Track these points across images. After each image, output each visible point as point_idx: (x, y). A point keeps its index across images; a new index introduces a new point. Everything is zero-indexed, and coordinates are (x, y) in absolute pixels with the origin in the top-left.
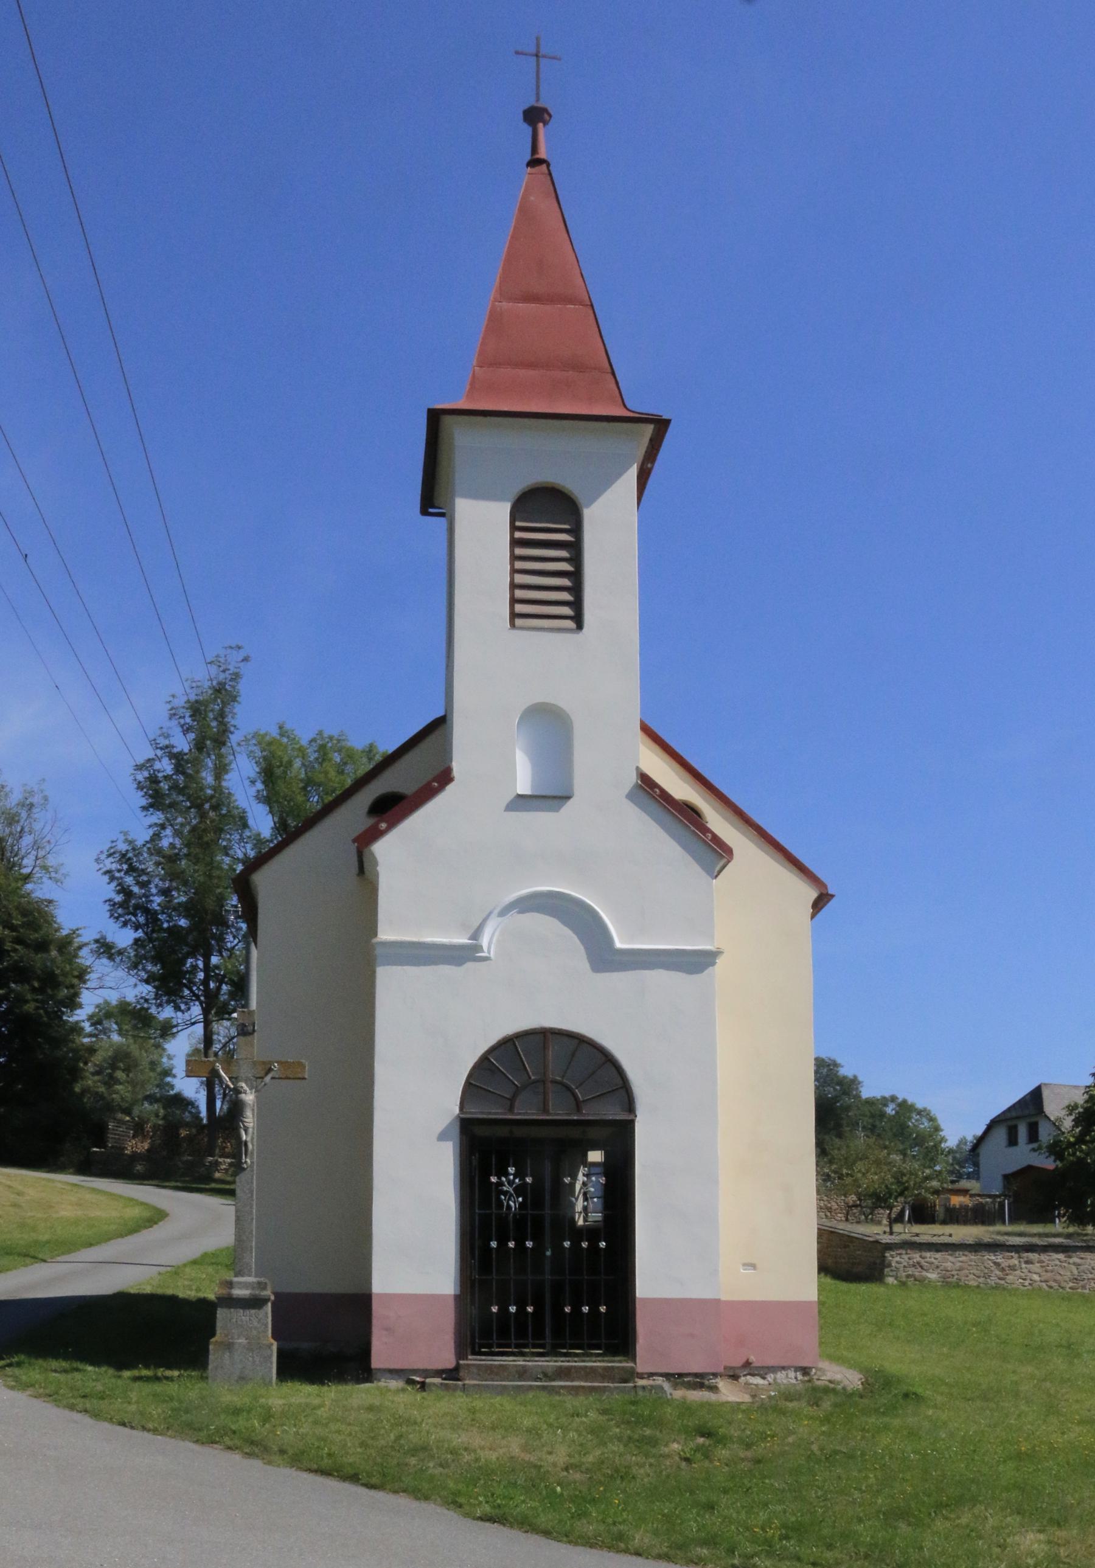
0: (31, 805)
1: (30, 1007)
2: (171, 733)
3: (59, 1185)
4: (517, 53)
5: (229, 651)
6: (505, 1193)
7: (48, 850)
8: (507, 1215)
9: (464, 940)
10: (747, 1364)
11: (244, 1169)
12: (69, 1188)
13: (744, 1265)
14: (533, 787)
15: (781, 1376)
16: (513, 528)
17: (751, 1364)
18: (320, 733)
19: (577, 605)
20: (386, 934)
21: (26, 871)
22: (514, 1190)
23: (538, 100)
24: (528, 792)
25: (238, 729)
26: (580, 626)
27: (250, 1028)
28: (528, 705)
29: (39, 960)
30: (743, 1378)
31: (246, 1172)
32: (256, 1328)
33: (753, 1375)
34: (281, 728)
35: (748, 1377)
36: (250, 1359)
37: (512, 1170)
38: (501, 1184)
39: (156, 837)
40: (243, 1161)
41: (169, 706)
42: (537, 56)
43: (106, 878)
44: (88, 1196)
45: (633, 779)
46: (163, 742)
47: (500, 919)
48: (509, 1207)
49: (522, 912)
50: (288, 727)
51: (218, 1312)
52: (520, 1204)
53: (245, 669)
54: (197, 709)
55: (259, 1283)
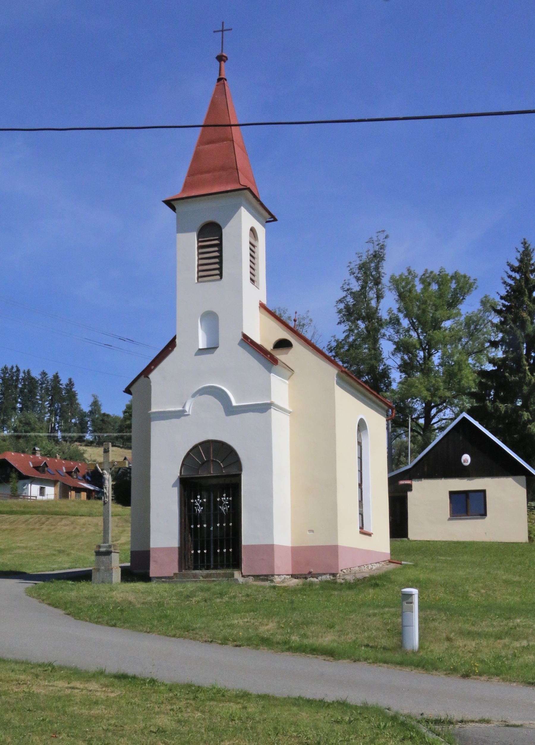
2: (350, 282)
4: (214, 32)
5: (379, 234)
6: (197, 506)
8: (197, 515)
9: (181, 409)
10: (310, 573)
13: (309, 531)
14: (207, 345)
15: (324, 578)
16: (199, 242)
17: (311, 572)
18: (426, 270)
19: (220, 269)
20: (154, 409)
22: (200, 505)
23: (222, 51)
24: (206, 347)
25: (386, 274)
26: (221, 278)
27: (107, 450)
28: (205, 311)
30: (309, 579)
33: (313, 577)
34: (408, 270)
35: (311, 578)
37: (199, 497)
38: (195, 502)
39: (348, 337)
41: (349, 269)
42: (222, 31)
45: (241, 337)
46: (346, 287)
47: (193, 399)
48: (198, 511)
49: (201, 395)
50: (412, 269)
52: (202, 510)
53: (388, 242)
54: (363, 267)
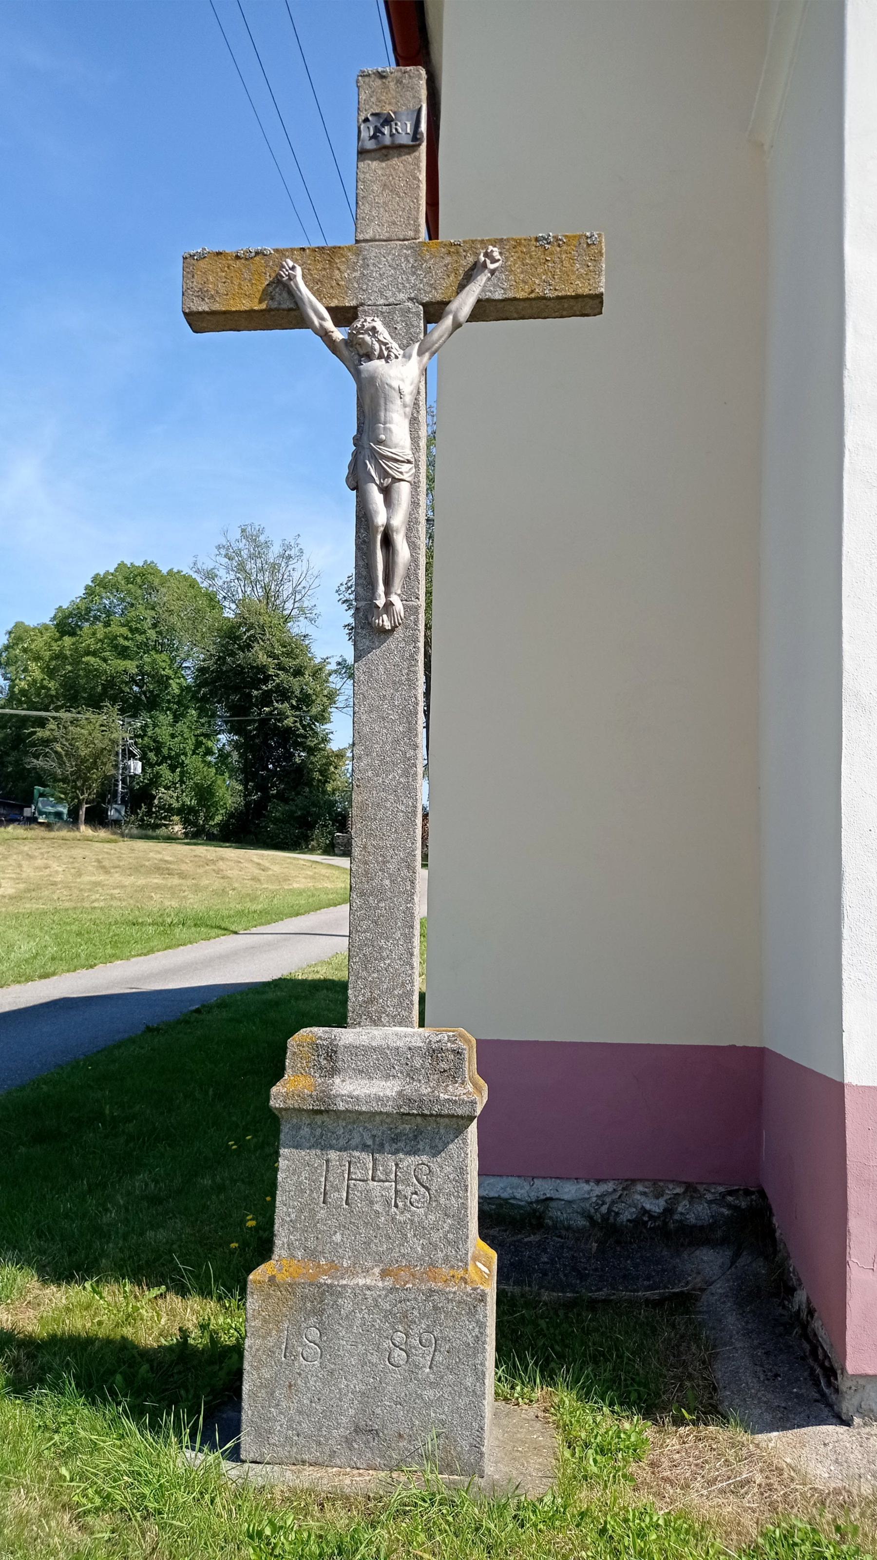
0: (290, 557)
1: (289, 722)
3: (302, 862)
7: (303, 594)
11: (386, 633)
12: (309, 864)
21: (286, 612)
29: (295, 684)
31: (391, 643)
32: (421, 1230)
36: (399, 1356)
40: (381, 602)
43: (345, 606)
44: (324, 871)
51: (282, 1163)
55: (434, 1052)
